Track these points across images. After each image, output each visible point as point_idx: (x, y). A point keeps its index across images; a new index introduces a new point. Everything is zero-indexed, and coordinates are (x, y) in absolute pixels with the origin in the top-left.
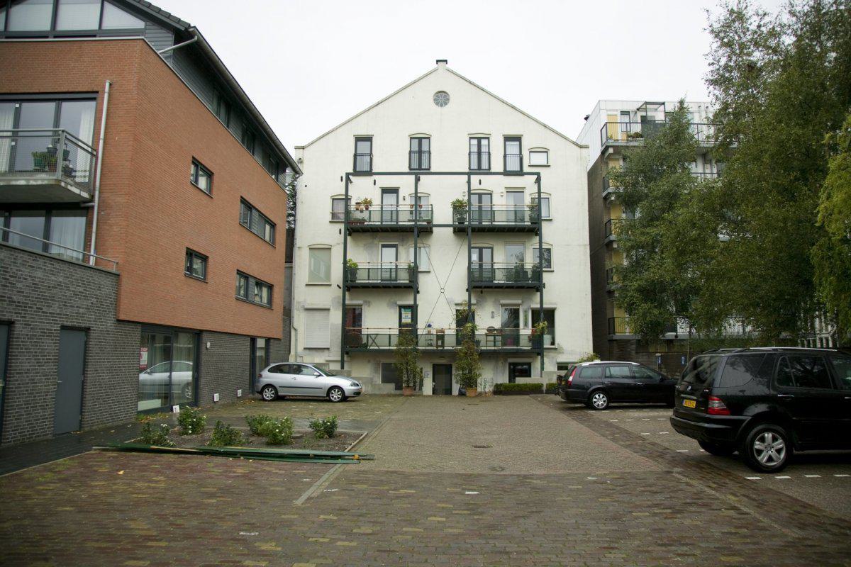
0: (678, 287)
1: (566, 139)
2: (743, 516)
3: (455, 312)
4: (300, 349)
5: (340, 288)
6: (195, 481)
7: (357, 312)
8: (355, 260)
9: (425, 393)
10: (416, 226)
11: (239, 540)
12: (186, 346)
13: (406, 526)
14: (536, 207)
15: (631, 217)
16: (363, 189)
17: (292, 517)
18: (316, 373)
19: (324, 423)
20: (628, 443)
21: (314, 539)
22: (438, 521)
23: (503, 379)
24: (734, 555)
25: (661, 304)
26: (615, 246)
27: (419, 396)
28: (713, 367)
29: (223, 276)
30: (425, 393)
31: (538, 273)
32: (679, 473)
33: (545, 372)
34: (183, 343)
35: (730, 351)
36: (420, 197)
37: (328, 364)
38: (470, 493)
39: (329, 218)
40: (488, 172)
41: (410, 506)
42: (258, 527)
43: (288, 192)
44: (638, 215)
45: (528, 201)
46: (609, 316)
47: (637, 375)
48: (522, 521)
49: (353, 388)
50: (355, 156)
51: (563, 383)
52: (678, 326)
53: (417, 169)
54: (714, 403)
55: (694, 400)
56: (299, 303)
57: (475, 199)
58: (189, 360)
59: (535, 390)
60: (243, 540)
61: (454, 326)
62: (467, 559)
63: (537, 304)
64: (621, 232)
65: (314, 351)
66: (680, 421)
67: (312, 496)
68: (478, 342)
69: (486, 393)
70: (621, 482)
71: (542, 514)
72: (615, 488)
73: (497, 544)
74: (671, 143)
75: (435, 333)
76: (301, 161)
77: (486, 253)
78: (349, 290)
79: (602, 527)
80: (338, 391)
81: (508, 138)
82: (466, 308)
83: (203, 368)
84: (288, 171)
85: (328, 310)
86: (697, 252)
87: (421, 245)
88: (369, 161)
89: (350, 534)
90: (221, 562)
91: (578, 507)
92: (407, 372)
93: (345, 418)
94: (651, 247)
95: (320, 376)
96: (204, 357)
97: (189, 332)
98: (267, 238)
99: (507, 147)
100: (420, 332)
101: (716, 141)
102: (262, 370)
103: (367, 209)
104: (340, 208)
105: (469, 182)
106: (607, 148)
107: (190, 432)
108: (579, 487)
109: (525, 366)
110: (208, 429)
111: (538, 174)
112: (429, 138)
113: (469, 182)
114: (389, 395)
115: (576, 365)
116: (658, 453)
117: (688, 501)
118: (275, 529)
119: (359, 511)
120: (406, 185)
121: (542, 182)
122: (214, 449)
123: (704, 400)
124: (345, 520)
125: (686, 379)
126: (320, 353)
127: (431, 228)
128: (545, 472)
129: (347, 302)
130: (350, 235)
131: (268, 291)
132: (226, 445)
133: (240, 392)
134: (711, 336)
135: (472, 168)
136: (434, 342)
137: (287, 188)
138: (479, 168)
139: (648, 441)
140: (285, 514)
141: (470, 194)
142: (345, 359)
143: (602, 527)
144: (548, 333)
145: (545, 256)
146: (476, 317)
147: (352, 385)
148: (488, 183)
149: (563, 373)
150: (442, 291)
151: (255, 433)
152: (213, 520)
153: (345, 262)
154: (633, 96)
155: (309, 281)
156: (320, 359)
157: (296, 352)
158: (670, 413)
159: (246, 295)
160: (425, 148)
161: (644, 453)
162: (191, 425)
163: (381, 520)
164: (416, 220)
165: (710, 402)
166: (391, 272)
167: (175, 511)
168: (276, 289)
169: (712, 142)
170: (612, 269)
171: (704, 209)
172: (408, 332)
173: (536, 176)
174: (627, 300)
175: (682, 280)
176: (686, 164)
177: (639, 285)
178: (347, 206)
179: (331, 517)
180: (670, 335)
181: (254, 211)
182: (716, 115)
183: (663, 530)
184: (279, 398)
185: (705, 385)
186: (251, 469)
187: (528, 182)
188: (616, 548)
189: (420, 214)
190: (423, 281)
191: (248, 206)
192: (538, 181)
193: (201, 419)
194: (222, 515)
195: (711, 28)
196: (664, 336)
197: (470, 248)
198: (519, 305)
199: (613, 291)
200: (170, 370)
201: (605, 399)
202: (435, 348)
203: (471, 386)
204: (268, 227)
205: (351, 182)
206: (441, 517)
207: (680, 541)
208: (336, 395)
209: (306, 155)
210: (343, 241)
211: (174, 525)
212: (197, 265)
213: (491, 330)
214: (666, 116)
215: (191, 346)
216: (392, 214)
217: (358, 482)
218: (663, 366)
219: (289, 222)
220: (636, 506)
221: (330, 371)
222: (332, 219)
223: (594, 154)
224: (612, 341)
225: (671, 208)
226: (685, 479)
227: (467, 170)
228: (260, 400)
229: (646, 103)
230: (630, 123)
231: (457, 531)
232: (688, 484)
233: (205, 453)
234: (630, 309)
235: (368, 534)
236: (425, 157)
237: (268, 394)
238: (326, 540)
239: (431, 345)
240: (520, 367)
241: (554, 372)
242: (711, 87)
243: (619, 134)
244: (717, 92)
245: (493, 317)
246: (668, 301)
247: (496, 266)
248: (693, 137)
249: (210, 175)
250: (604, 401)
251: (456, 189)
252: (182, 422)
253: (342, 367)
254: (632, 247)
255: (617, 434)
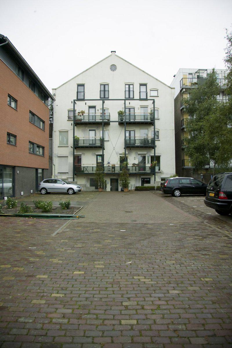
0: (210, 147)
1: (165, 85)
2: (230, 239)
3: (119, 157)
4: (56, 173)
5: (72, 148)
6: (12, 227)
7: (80, 158)
8: (78, 136)
9: (107, 190)
10: (103, 122)
11: (29, 250)
12: (9, 172)
13: (95, 244)
14: (153, 114)
15: (192, 118)
16: (81, 107)
17: (50, 241)
18: (62, 183)
19: (65, 203)
20: (188, 210)
21: (58, 250)
22: (109, 242)
23: (139, 184)
24: (225, 255)
25: (204, 154)
26: (185, 130)
27: (105, 191)
28: (222, 180)
29: (23, 143)
30: (107, 190)
31: (153, 141)
32: (207, 222)
33: (156, 181)
34: (8, 171)
35: (229, 174)
36: (105, 110)
37: (68, 179)
38: (122, 230)
39: (67, 118)
40: (133, 99)
41: (97, 236)
42: (36, 245)
43: (50, 108)
44: (195, 117)
45: (149, 111)
46: (182, 159)
47: (192, 183)
48: (142, 241)
49: (78, 189)
50: (77, 92)
51: (163, 186)
52: (210, 163)
53: (103, 98)
54: (221, 195)
55: (213, 193)
56: (55, 154)
57: (127, 110)
58: (10, 178)
59: (152, 189)
60: (30, 250)
61: (119, 163)
62: (119, 257)
63: (153, 154)
64: (188, 125)
65: (62, 174)
66: (208, 202)
67: (59, 232)
68: (129, 170)
69: (132, 190)
70: (183, 226)
71: (150, 239)
72: (180, 228)
73: (131, 251)
74: (209, 87)
75: (111, 166)
76: (55, 95)
77: (132, 133)
78: (76, 149)
79: (174, 244)
80: (72, 190)
81: (141, 85)
82: (124, 156)
83: (16, 181)
84: (49, 99)
85: (68, 157)
86: (218, 133)
87: (105, 130)
88: (83, 94)
89: (74, 247)
90: (21, 259)
91: (165, 236)
92: (100, 182)
93: (74, 201)
94: (200, 129)
95: (64, 184)
96: (16, 177)
97: (11, 167)
98: (41, 127)
99: (141, 88)
100: (105, 166)
101: (228, 86)
102: (41, 182)
103: (83, 115)
104: (72, 115)
105: (125, 103)
106: (182, 89)
107: (11, 207)
108: (166, 228)
109: (148, 179)
110: (18, 206)
111: (154, 100)
112: (108, 85)
113: (125, 103)
114: (92, 191)
115: (168, 179)
116: (199, 214)
117: (209, 233)
118: (43, 246)
119: (77, 238)
120: (99, 104)
121: (155, 103)
122: (20, 214)
123: (217, 194)
124: (71, 242)
125: (211, 185)
126: (65, 175)
127: (109, 123)
128: (153, 222)
129: (75, 154)
130: (76, 126)
131: (42, 150)
132: (25, 212)
133: (32, 191)
134: (223, 167)
135: (126, 97)
136: (111, 170)
137: (49, 106)
138: (129, 98)
139: (196, 210)
140: (47, 240)
141: (125, 108)
142: (75, 177)
143: (174, 244)
144: (157, 166)
145: (156, 134)
146: (128, 160)
147: (77, 188)
148: (133, 103)
149: (163, 182)
150: (114, 148)
151: (38, 208)
152: (19, 243)
153: (74, 137)
154: (194, 66)
155: (59, 145)
156: (64, 177)
157: (55, 174)
158: (204, 198)
159: (33, 151)
160: (107, 89)
161: (194, 214)
162: (11, 205)
163: (86, 242)
164: (103, 119)
165: (220, 194)
166: (93, 141)
167: (3, 239)
168: (45, 149)
169: (226, 87)
170: (184, 140)
171: (221, 115)
172: (100, 166)
173: (153, 101)
174: (190, 152)
175: (212, 144)
176: (215, 96)
177: (195, 146)
178: (74, 113)
179: (67, 241)
180: (207, 167)
181: (35, 116)
182: (228, 75)
183: (198, 245)
184: (48, 193)
185: (218, 187)
186: (35, 222)
187: (149, 103)
188: (179, 252)
189: (105, 117)
190: (106, 144)
191: (33, 114)
192: (154, 103)
193: (15, 202)
194: (22, 241)
195: (227, 37)
196: (204, 167)
197: (125, 131)
198: (145, 154)
199: (184, 149)
200: (3, 183)
201: (180, 192)
202: (111, 172)
203: (126, 188)
204: (41, 123)
205: (76, 104)
206: (110, 240)
207: (204, 249)
208: (71, 192)
209: (57, 93)
210: (73, 128)
211: (3, 245)
212: (12, 139)
213: (134, 164)
214: (207, 76)
215: (11, 172)
216: (93, 117)
217: (78, 227)
218: (204, 179)
219: (50, 121)
220: (188, 236)
221: (69, 182)
222: (68, 119)
223: (177, 91)
224: (183, 169)
225: (208, 114)
226: (209, 225)
227: (124, 98)
228: (40, 194)
229: (199, 70)
230: (192, 78)
231: (116, 246)
232: (210, 227)
233: (16, 216)
234: (191, 156)
235: (80, 247)
236: (107, 93)
237: (43, 192)
238: (63, 250)
239: (110, 171)
240: (146, 180)
241: (160, 182)
242: (226, 63)
243: (188, 83)
244: (229, 65)
245: (135, 159)
246: (206, 153)
247: (136, 138)
248: (218, 84)
249: (16, 101)
250: (179, 193)
251: (119, 106)
252: (8, 203)
253: (74, 180)
254: (192, 130)
255: (183, 206)
